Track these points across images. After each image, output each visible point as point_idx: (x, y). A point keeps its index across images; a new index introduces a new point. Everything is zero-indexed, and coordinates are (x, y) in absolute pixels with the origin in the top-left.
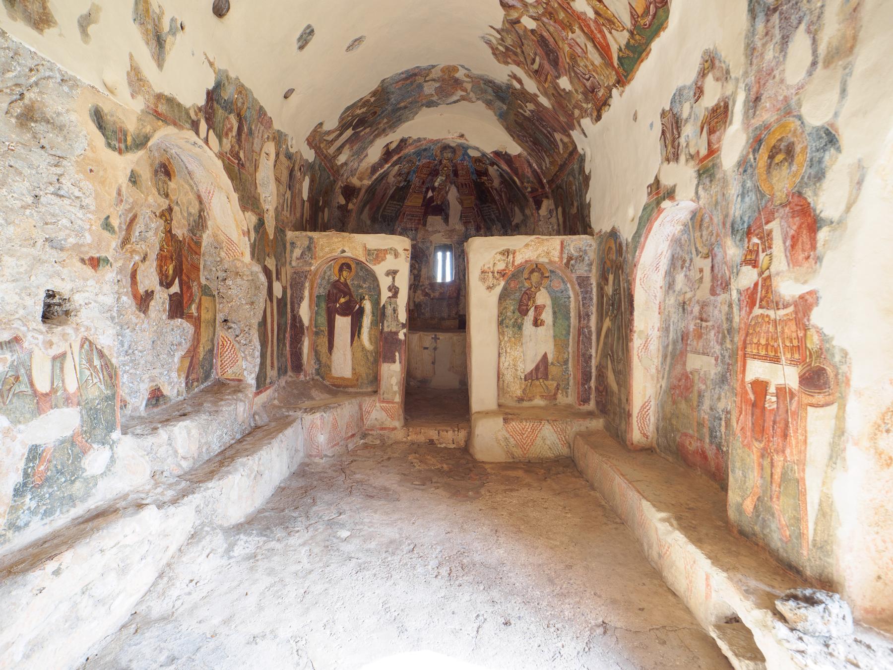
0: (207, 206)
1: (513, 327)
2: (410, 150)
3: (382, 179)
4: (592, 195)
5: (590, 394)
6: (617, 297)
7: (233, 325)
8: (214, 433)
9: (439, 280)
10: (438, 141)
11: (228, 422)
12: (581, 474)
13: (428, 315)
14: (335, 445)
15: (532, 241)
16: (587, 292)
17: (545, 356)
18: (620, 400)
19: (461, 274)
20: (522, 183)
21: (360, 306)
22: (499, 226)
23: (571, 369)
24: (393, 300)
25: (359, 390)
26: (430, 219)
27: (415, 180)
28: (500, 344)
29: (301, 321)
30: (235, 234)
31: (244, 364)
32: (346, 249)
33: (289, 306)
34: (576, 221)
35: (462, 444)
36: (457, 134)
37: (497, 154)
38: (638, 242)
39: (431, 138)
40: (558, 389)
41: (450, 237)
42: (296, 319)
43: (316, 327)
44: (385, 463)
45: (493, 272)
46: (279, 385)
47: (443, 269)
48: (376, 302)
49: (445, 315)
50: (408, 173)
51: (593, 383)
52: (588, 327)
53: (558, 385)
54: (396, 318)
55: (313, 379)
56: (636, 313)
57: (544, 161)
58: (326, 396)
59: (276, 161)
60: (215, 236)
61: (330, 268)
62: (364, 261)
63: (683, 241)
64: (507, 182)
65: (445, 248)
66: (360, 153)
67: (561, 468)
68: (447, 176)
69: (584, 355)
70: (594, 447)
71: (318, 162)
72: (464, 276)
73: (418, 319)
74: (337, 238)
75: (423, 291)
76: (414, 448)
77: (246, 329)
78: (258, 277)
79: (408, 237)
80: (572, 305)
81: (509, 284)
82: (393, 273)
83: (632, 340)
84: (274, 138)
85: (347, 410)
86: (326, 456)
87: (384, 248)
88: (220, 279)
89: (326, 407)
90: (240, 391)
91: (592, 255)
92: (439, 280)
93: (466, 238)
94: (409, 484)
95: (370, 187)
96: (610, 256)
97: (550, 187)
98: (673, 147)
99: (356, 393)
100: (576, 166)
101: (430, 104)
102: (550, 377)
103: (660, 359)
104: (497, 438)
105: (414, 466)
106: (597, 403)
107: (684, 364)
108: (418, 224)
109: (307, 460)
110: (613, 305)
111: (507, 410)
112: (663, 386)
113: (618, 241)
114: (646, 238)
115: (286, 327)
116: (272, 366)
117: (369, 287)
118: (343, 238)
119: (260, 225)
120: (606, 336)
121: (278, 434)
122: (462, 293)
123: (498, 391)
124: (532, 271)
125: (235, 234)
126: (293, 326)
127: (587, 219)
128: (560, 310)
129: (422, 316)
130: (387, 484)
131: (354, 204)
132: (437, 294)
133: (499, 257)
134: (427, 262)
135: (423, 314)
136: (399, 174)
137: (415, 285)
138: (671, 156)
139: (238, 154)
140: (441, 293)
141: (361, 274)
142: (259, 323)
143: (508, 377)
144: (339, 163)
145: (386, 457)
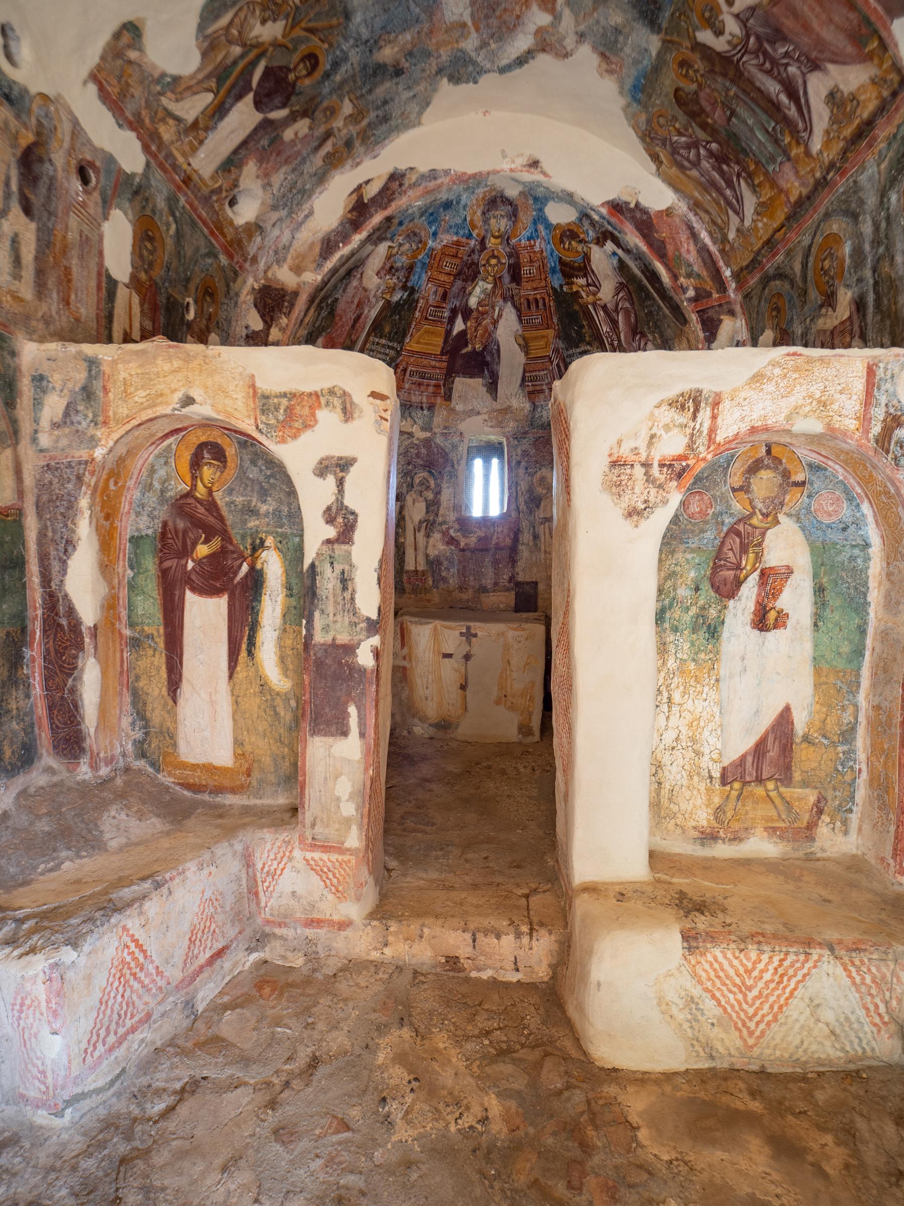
1: (694, 630)
2: (410, 201)
9: (476, 512)
10: (478, 179)
15: (774, 364)
20: (675, 277)
21: (252, 568)
23: (861, 756)
24: (340, 549)
25: (254, 801)
26: (461, 383)
27: (428, 291)
29: (71, 611)
32: (196, 393)
35: (542, 973)
36: (521, 161)
37: (617, 207)
40: (820, 812)
41: (500, 424)
42: (56, 605)
43: (132, 625)
45: (646, 465)
48: (293, 554)
50: (411, 269)
55: (127, 770)
58: (155, 824)
65: (489, 450)
66: (293, 201)
68: (497, 281)
74: (169, 359)
75: (445, 533)
76: (404, 1000)
82: (337, 467)
92: (476, 512)
95: (319, 289)
97: (739, 288)
99: (246, 810)
101: (461, 70)
102: (797, 776)
104: (660, 1000)
108: (435, 394)
117: (277, 513)
118: (188, 359)
124: (755, 468)
126: (51, 625)
131: (283, 330)
132: (472, 540)
133: (668, 415)
134: (453, 475)
135: (445, 580)
136: (390, 269)
140: (480, 539)
141: (253, 473)
143: (674, 774)
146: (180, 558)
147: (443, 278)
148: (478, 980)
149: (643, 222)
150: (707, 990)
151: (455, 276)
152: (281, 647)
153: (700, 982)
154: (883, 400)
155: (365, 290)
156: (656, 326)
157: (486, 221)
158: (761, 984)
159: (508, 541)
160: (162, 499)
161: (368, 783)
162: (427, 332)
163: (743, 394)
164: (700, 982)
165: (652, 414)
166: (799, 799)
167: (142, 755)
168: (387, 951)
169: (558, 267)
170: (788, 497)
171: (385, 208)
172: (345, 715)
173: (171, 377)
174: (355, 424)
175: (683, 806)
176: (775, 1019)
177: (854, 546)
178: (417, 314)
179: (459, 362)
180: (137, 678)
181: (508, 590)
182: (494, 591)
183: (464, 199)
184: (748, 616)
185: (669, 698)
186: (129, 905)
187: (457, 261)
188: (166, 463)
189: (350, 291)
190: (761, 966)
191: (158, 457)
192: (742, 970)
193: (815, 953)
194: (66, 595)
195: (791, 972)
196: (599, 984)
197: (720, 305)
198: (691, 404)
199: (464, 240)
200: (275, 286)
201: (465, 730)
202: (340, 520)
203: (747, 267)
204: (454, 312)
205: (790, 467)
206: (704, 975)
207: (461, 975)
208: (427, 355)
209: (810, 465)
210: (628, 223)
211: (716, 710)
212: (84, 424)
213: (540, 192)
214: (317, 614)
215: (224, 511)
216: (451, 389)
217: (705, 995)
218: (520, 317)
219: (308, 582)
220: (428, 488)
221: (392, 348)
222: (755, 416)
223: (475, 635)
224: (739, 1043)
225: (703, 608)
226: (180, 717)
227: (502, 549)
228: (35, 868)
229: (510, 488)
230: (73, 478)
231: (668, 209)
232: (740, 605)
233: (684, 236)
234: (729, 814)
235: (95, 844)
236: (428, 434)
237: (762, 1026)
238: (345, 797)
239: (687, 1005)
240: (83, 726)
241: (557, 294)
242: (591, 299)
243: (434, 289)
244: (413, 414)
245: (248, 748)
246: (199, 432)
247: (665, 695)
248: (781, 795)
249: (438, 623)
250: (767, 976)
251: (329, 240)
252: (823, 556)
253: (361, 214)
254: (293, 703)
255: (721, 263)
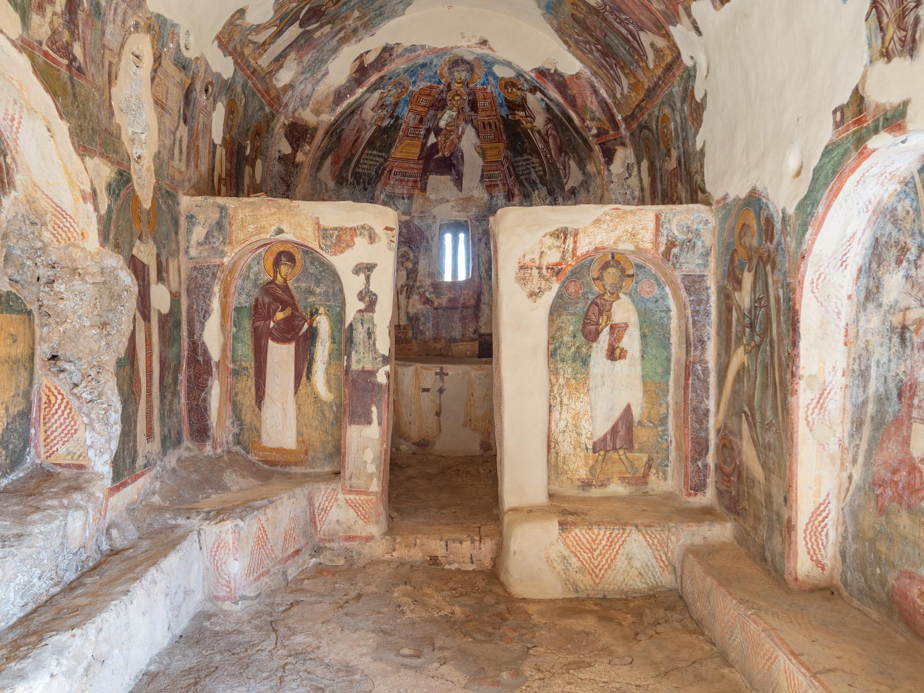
0: (12, 145)
1: (574, 361)
2: (397, 66)
3: (353, 112)
4: (707, 136)
5: (705, 476)
6: (761, 313)
7: (67, 366)
8: (11, 580)
9: (448, 278)
10: (444, 51)
11: (43, 555)
12: (698, 628)
13: (429, 334)
14: (263, 575)
15: (606, 214)
16: (700, 302)
17: (628, 410)
18: (769, 496)
19: (483, 269)
20: (583, 120)
21: (311, 326)
22: (544, 191)
23: (671, 432)
24: (367, 315)
26: (433, 179)
27: (408, 117)
28: (552, 391)
29: (206, 352)
30: (68, 200)
31: (89, 437)
32: (285, 227)
33: (184, 327)
34: (674, 179)
35: (487, 563)
36: (474, 41)
37: (542, 73)
38: (811, 214)
39: (433, 45)
40: (650, 467)
41: (464, 209)
42: (197, 348)
43: (234, 361)
44: (352, 607)
45: (539, 268)
46: (164, 468)
47: (454, 261)
48: (338, 318)
49: (457, 334)
50: (396, 104)
51: (711, 459)
52: (703, 362)
53: (650, 459)
54: (373, 348)
55: (229, 452)
56: (803, 344)
57: (620, 84)
58: (251, 482)
59: (155, 71)
60: (31, 201)
61: (258, 259)
62: (314, 245)
63: (900, 212)
64: (558, 120)
65: (457, 227)
66: (315, 68)
67: (661, 612)
68: (460, 110)
69: (695, 410)
70: (726, 581)
71: (240, 80)
72: (489, 270)
73: (409, 343)
74: (269, 207)
75: (422, 295)
76: (405, 574)
77: (93, 373)
78: (116, 278)
79: (397, 209)
80: (674, 324)
81: (567, 288)
82: (366, 269)
83: (794, 392)
84: (149, 28)
85: (285, 510)
86: (244, 598)
87: (350, 225)
88: (43, 281)
89: (245, 508)
90: (78, 489)
91: (708, 238)
92: (448, 278)
93: (492, 210)
94: (392, 656)
96: (747, 240)
97: (627, 128)
98: (900, 27)
99: (305, 475)
100: (677, 90)
102: (636, 446)
103: (848, 427)
104: (548, 558)
105: (403, 612)
106: (720, 493)
107: (906, 442)
108: (414, 187)
109: (209, 605)
110: (752, 326)
111: (565, 505)
112: (856, 477)
113: (764, 213)
114: (828, 207)
115: (179, 363)
116: (150, 435)
117: (326, 293)
118: (280, 208)
119: (122, 181)
120: (738, 379)
121: (146, 570)
122: (485, 298)
123: (549, 471)
124: (605, 266)
125: (68, 200)
127: (697, 178)
128: (653, 331)
129: (419, 336)
130: (352, 657)
131: (306, 154)
132: (444, 301)
133: (550, 241)
134: (428, 249)
135: (422, 332)
137: (407, 287)
138: (896, 46)
139: (66, 51)
141: (312, 270)
142: (120, 363)
143: (565, 446)
144: (280, 85)
145: (353, 594)
146: (265, 321)
147: (420, 109)
148: (450, 570)
149: (560, 83)
150: (572, 552)
151: (429, 108)
152: (327, 373)
153: (568, 547)
154: (665, 233)
155: (363, 121)
156: (574, 148)
157: (451, 73)
158: (600, 548)
159: (473, 302)
160: (255, 284)
161: (383, 452)
162: (408, 144)
163: (590, 230)
164: (568, 547)
165: (541, 240)
166: (638, 460)
167: (238, 442)
168: (395, 554)
169: (504, 103)
170: (624, 283)
171: (380, 71)
172: (370, 412)
173: (270, 218)
174: (376, 245)
175: (571, 467)
176: (609, 567)
177: (662, 311)
178: (401, 133)
179: (432, 164)
180: (236, 394)
181: (473, 340)
182: (462, 341)
183: (435, 61)
184: (604, 353)
185: (561, 401)
186: (261, 508)
187: (431, 98)
188: (258, 263)
189: (353, 123)
190: (600, 537)
191: (253, 260)
192: (590, 540)
193: (628, 529)
194: (203, 343)
195: (616, 540)
196: (515, 552)
197: (615, 139)
198: (562, 235)
199: (435, 85)
200: (300, 123)
201: (442, 446)
202: (367, 299)
203: (630, 116)
204: (428, 131)
205: (625, 266)
206: (570, 543)
207: (439, 567)
208: (408, 160)
209: (637, 265)
210: (549, 84)
211: (588, 408)
212: (217, 244)
213: (489, 59)
214: (353, 353)
215: (294, 292)
216: (426, 184)
217: (572, 555)
218: (478, 134)
219: (348, 335)
220: (408, 259)
221: (382, 157)
222: (597, 242)
223: (447, 374)
224: (591, 582)
225: (578, 348)
226: (263, 418)
227: (467, 307)
228: (198, 496)
229: (473, 259)
230: (210, 275)
231: (577, 74)
232: (599, 346)
233: (588, 92)
234: (598, 470)
235: (222, 487)
236: (408, 218)
237: (603, 571)
238: (369, 462)
239: (562, 561)
240: (209, 422)
241: (505, 120)
242: (529, 125)
243: (413, 116)
244: (396, 203)
245: (306, 437)
246: (279, 245)
247: (559, 399)
248: (627, 457)
249: (418, 365)
250: (604, 543)
251: (340, 92)
252: (645, 317)
253: (362, 75)
254: (335, 408)
255: (615, 111)
